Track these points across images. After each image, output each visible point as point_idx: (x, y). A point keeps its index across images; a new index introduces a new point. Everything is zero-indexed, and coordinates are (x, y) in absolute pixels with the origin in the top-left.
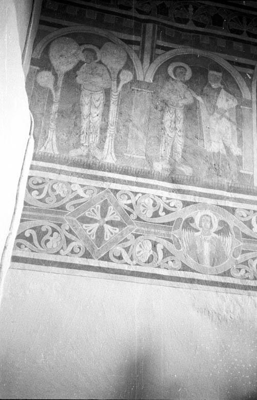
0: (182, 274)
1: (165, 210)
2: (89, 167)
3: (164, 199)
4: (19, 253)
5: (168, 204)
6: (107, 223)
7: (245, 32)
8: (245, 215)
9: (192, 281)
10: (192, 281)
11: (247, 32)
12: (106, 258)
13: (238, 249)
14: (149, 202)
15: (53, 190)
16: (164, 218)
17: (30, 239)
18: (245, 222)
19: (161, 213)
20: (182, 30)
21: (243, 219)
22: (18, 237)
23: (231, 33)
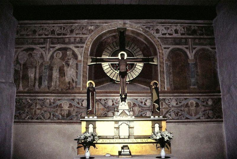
0: (186, 120)
1: (116, 103)
2: (30, 93)
3: (115, 99)
4: (16, 120)
5: (180, 100)
6: (37, 109)
7: (81, 34)
8: (77, 101)
9: (189, 122)
10: (189, 122)
11: (168, 33)
12: (37, 119)
13: (139, 111)
14: (48, 101)
15: (22, 102)
16: (53, 105)
17: (18, 116)
18: (77, 103)
19: (115, 104)
20: (59, 38)
21: (77, 102)
22: (15, 116)
23: (188, 35)
